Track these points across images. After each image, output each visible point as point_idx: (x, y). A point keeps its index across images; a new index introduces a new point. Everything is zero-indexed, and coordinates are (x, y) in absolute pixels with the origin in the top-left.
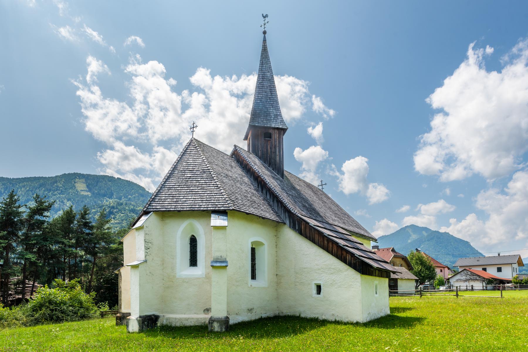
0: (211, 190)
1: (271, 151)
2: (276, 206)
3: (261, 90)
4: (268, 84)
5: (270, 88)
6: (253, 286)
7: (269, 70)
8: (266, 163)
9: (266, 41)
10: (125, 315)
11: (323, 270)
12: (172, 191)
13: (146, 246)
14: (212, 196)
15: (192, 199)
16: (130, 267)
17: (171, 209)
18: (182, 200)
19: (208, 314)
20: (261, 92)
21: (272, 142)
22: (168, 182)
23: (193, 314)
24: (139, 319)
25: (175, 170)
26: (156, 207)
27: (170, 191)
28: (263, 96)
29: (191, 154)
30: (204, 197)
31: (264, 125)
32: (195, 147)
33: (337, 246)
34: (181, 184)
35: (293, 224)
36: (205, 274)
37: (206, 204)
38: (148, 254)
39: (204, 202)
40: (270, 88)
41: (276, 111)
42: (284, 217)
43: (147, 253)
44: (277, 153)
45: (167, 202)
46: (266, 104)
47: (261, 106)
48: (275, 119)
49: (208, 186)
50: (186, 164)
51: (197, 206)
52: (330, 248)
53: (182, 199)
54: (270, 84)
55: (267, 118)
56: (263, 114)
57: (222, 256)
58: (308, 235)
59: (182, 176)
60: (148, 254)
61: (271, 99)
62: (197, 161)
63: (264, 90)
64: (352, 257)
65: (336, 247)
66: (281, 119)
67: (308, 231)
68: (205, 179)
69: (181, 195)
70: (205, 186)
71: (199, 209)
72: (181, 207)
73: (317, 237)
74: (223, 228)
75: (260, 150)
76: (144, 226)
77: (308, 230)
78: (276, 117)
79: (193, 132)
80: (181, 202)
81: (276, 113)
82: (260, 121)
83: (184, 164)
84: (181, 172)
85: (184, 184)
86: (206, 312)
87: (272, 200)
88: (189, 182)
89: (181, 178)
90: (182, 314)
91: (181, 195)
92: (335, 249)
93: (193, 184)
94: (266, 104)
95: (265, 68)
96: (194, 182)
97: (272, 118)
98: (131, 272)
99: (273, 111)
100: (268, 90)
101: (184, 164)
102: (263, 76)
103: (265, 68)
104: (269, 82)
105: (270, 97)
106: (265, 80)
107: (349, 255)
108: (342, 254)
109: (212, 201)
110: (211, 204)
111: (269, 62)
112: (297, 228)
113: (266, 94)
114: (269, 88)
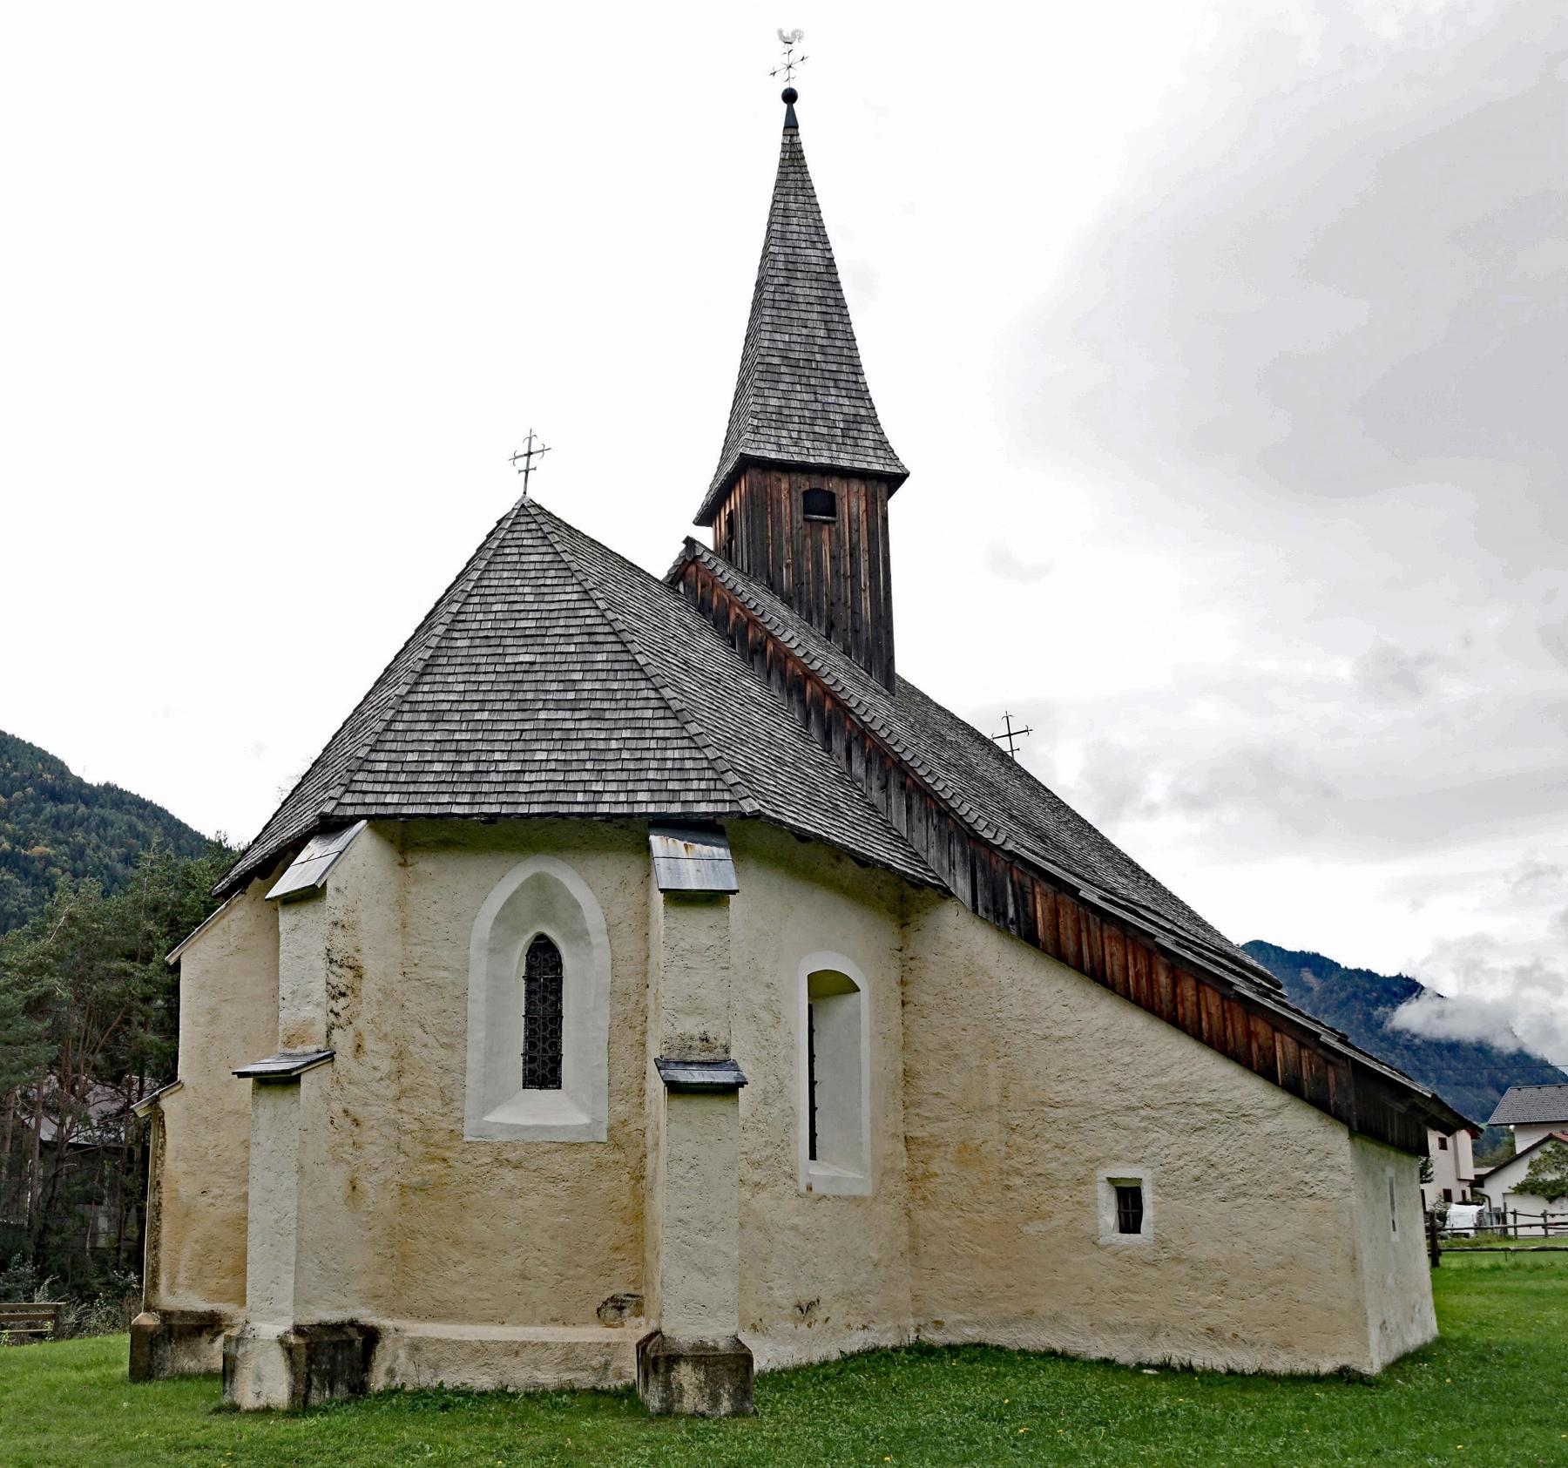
0: (639, 724)
1: (837, 572)
2: (899, 813)
3: (783, 313)
4: (814, 292)
5: (824, 309)
6: (818, 1189)
7: (815, 238)
8: (815, 621)
9: (796, 127)
10: (175, 1322)
11: (1154, 1114)
12: (453, 726)
13: (334, 980)
14: (649, 749)
15: (552, 765)
16: (250, 1080)
17: (456, 810)
18: (501, 767)
19: (622, 1325)
20: (787, 321)
21: (837, 530)
22: (426, 688)
23: (544, 1323)
24: (292, 1339)
25: (456, 635)
26: (382, 799)
27: (439, 726)
28: (794, 338)
29: (525, 567)
30: (610, 756)
31: (804, 459)
32: (540, 534)
33: (1223, 997)
34: (492, 696)
35: (988, 894)
36: (605, 1125)
37: (622, 787)
38: (342, 1021)
39: (610, 776)
40: (824, 309)
41: (854, 402)
42: (941, 866)
43: (337, 1015)
44: (864, 578)
45: (431, 778)
46: (807, 372)
47: (787, 379)
48: (851, 433)
49: (622, 704)
50: (505, 607)
51: (580, 797)
52: (1188, 1004)
53: (504, 761)
54: (820, 293)
55: (817, 429)
56: (799, 413)
57: (711, 1035)
58: (1070, 946)
59: (490, 660)
60: (342, 1021)
61: (830, 350)
62: (557, 598)
63: (794, 315)
64: (1301, 1045)
65: (1218, 1002)
66: (877, 437)
67: (1070, 924)
68: (603, 676)
69: (497, 746)
70: (606, 705)
71: (591, 809)
72: (503, 798)
73: (1114, 955)
74: (714, 899)
75: (787, 566)
76: (329, 885)
77: (1067, 922)
78: (855, 426)
79: (527, 472)
80: (500, 778)
81: (853, 411)
82: (784, 441)
83: (495, 608)
84: (485, 642)
85: (506, 696)
86: (611, 1313)
87: (875, 784)
88: (526, 687)
89: (491, 668)
90: (490, 1320)
91: (497, 746)
92: (1213, 1010)
93: (549, 697)
94: (807, 372)
95: (797, 229)
96: (554, 686)
97: (839, 432)
98: (255, 1104)
99: (841, 401)
100: (815, 316)
101: (495, 608)
102: (792, 259)
103: (797, 229)
104: (815, 284)
105: (825, 342)
106: (799, 275)
107: (1289, 1040)
108: (1250, 1035)
109: (651, 775)
110: (645, 786)
111: (814, 209)
112: (1011, 912)
113: (804, 331)
114: (817, 308)
